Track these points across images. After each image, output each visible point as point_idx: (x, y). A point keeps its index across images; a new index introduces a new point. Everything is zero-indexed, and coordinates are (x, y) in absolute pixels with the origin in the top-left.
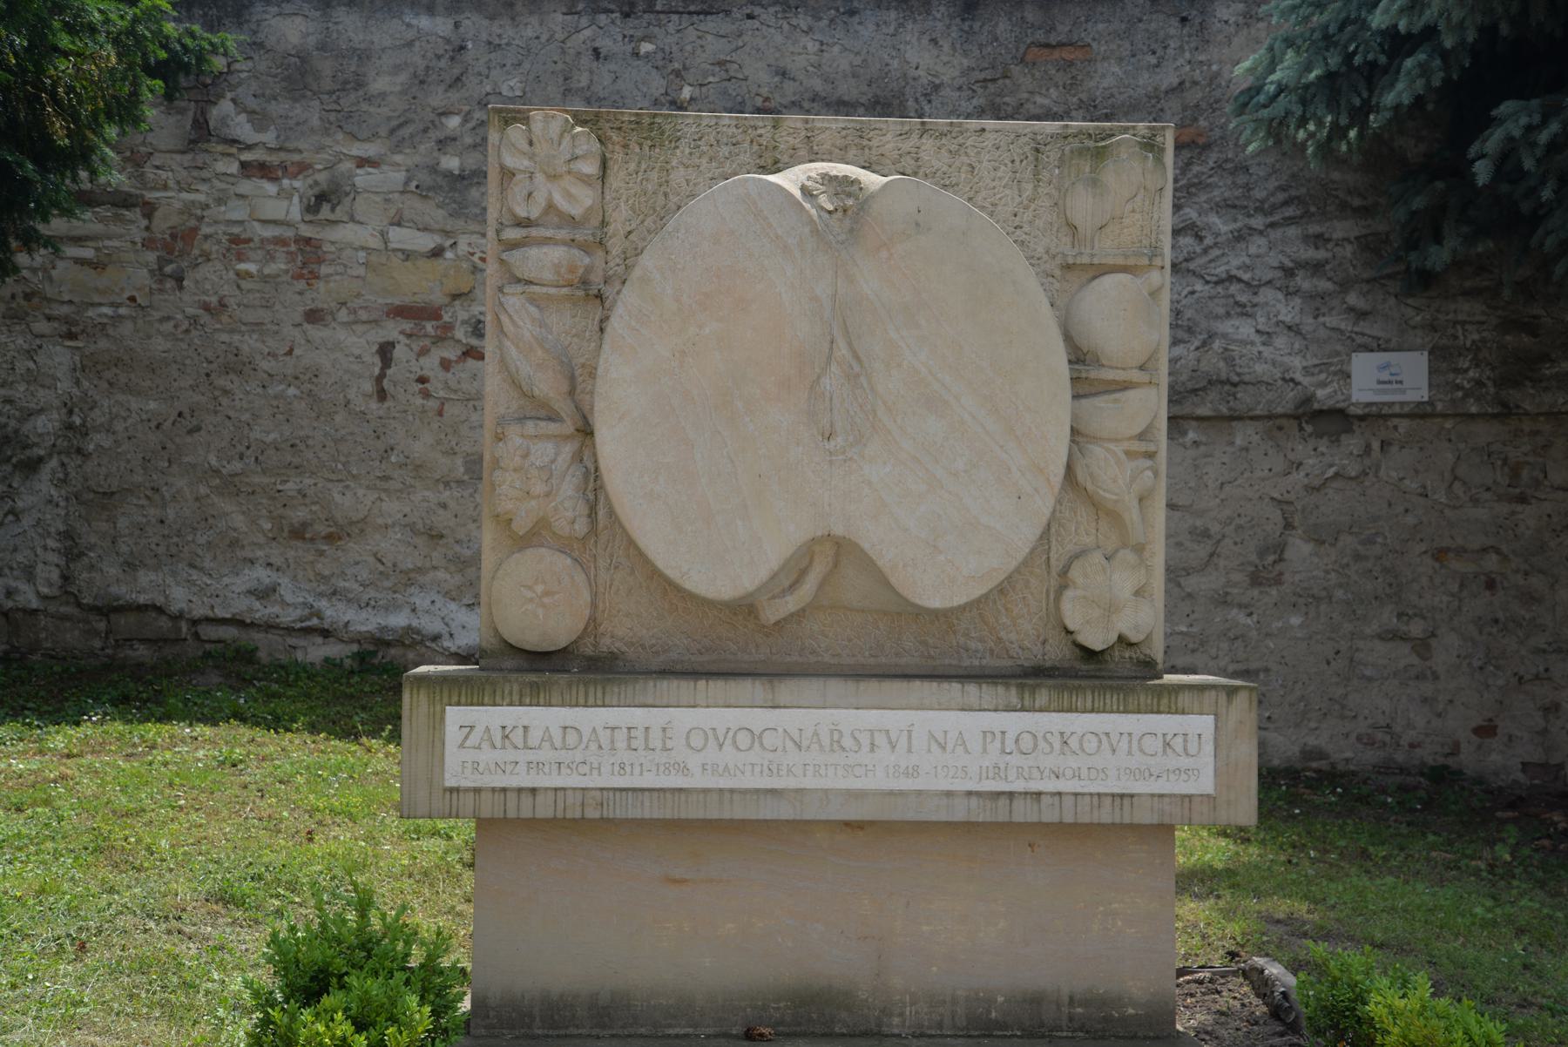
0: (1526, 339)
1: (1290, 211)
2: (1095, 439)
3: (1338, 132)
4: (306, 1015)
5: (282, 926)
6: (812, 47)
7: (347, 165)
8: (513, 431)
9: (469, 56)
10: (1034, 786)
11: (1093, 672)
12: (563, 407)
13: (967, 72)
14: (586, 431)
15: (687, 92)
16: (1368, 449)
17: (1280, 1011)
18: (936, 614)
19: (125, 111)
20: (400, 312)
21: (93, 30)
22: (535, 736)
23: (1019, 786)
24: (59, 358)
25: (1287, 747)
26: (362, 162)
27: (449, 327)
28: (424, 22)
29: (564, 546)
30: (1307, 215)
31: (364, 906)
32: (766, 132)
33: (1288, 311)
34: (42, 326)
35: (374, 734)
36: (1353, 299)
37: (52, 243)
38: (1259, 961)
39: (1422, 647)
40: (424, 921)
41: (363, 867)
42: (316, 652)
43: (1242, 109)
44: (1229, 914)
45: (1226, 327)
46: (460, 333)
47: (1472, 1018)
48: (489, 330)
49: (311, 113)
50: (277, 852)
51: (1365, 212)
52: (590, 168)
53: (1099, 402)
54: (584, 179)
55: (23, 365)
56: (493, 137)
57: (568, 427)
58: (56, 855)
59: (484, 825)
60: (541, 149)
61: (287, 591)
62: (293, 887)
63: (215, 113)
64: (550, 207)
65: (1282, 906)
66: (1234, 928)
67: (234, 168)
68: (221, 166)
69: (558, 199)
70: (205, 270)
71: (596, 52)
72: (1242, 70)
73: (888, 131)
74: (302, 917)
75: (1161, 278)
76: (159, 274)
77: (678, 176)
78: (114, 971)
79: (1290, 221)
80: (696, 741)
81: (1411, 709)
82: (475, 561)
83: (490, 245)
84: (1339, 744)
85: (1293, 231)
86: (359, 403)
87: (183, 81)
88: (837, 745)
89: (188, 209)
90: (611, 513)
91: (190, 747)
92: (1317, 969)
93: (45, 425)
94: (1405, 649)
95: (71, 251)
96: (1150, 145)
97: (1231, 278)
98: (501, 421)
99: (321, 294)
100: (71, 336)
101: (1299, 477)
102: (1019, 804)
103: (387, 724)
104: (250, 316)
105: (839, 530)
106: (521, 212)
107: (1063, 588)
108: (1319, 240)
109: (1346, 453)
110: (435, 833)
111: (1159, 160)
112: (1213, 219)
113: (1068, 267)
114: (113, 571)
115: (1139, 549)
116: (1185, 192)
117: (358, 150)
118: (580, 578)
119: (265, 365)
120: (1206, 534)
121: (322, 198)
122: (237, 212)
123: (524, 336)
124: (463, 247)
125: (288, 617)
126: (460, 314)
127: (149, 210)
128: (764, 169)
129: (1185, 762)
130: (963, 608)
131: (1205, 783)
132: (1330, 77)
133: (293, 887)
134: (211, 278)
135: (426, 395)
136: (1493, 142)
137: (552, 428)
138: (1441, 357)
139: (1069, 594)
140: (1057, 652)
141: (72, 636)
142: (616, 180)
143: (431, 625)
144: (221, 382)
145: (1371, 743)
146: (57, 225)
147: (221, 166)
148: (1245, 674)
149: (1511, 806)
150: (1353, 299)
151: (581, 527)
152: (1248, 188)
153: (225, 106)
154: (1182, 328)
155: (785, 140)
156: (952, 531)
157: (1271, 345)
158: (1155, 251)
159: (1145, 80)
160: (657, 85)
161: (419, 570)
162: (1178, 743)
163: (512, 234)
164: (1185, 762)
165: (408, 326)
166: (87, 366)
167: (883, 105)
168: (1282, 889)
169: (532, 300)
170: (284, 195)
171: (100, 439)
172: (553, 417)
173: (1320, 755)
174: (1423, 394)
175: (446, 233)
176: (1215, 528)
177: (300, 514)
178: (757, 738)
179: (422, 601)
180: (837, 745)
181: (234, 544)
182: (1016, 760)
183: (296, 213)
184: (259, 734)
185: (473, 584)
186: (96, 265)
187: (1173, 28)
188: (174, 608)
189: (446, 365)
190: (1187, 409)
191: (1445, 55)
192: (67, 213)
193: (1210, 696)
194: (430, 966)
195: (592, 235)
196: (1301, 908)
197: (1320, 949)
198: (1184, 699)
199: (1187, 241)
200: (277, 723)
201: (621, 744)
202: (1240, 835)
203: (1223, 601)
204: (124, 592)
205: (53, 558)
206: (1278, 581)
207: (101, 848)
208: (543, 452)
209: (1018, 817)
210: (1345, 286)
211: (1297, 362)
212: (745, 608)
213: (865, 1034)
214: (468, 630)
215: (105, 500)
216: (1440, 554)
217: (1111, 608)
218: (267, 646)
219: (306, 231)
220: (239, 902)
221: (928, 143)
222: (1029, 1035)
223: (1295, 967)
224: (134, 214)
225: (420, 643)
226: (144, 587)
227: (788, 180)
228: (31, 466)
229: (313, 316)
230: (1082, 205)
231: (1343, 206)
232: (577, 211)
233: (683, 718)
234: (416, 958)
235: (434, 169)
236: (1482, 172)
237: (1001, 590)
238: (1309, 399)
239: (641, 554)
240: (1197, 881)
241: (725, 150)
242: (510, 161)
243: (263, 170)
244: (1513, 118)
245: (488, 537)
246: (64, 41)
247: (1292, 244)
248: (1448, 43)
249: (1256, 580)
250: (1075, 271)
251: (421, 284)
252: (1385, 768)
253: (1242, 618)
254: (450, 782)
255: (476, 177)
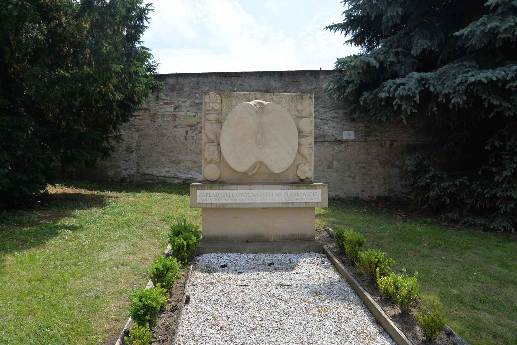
0: (369, 129)
1: (333, 108)
2: (302, 145)
3: (340, 96)
4: (176, 238)
5: (172, 225)
6: (256, 82)
7: (180, 102)
8: (207, 145)
9: (200, 84)
10: (293, 202)
11: (302, 183)
12: (215, 141)
13: (281, 86)
14: (219, 145)
15: (235, 89)
16: (345, 146)
17: (331, 236)
18: (277, 174)
19: (146, 95)
20: (189, 126)
21: (141, 83)
22: (211, 194)
23: (290, 202)
24: (136, 135)
25: (333, 195)
26: (183, 102)
27: (197, 128)
28: (193, 79)
29: (216, 163)
30: (335, 109)
31: (185, 221)
32: (248, 95)
33: (333, 124)
34: (133, 130)
35: (186, 194)
36: (343, 122)
37: (135, 116)
38: (328, 228)
39: (354, 178)
40: (194, 224)
41: (185, 216)
42: (176, 181)
43: (325, 92)
44: (323, 221)
45: (323, 127)
46: (198, 129)
47: (359, 235)
48: (203, 128)
49: (175, 94)
50: (171, 213)
51: (344, 109)
52: (219, 101)
53: (303, 139)
54: (218, 103)
55: (130, 136)
56: (203, 97)
57: (216, 144)
58: (138, 213)
59: (204, 209)
60: (211, 98)
61: (171, 171)
62: (174, 218)
63: (160, 95)
64: (213, 108)
65: (332, 219)
66: (324, 223)
67: (163, 103)
68: (161, 103)
69: (214, 107)
70: (158, 120)
71: (220, 83)
72: (325, 86)
73: (268, 95)
74: (175, 223)
75: (312, 119)
76: (151, 121)
77: (234, 103)
78: (147, 231)
79: (333, 110)
80: (238, 195)
81: (352, 188)
82: (201, 166)
83: (203, 114)
84: (341, 194)
85: (333, 112)
86: (182, 141)
87: (155, 90)
88: (261, 195)
89: (155, 110)
90: (223, 158)
91: (157, 196)
92: (337, 229)
93: (134, 145)
94: (351, 178)
95: (138, 118)
96: (310, 97)
97: (324, 119)
98: (205, 143)
99: (176, 123)
100: (138, 131)
101: (335, 151)
102: (290, 204)
103: (187, 193)
104: (165, 127)
105: (261, 160)
106: (208, 109)
107: (297, 169)
108: (337, 113)
109: (342, 147)
110: (196, 210)
111: (312, 100)
112: (321, 109)
113: (297, 117)
114: (145, 168)
115: (310, 163)
116: (316, 106)
117: (182, 100)
118: (218, 169)
119: (168, 135)
120: (320, 160)
121: (176, 108)
122: (163, 110)
123: (208, 129)
124: (199, 115)
125: (172, 176)
126: (198, 126)
127: (150, 110)
128: (248, 101)
129: (317, 197)
130: (281, 173)
131: (320, 200)
132: (338, 87)
133: (174, 218)
134: (159, 121)
135: (193, 139)
136: (363, 98)
137: (213, 144)
138: (356, 132)
139: (298, 170)
140: (296, 180)
141: (139, 179)
142: (223, 103)
143: (195, 177)
144: (161, 138)
145: (346, 193)
146: (136, 114)
147: (161, 103)
148: (327, 183)
149: (366, 203)
150: (343, 122)
151: (218, 160)
152: (326, 105)
153: (161, 94)
154: (316, 127)
155: (251, 96)
156: (279, 160)
157: (330, 130)
158: (311, 115)
159: (309, 87)
160: (230, 88)
161: (193, 168)
162: (316, 194)
163: (207, 112)
164: (317, 197)
165: (190, 128)
166: (140, 136)
167: (267, 91)
168: (332, 217)
169: (210, 123)
170: (171, 107)
171: (142, 147)
172: (213, 142)
173: (338, 196)
174: (354, 138)
175: (196, 113)
176: (322, 160)
177: (173, 159)
178: (247, 194)
179: (193, 173)
180: (261, 195)
181: (163, 164)
182: (290, 197)
183: (172, 110)
184: (168, 194)
185: (201, 170)
186: (142, 120)
187: (314, 79)
188: (154, 174)
189: (196, 134)
190: (317, 140)
191: (355, 84)
192: (137, 111)
193: (321, 186)
194: (195, 231)
195: (220, 112)
196: (335, 220)
197: (337, 226)
198: (317, 187)
199: (317, 113)
200: (171, 193)
201: (225, 196)
202: (325, 208)
203: (323, 171)
204: (146, 172)
205: (135, 166)
206: (332, 168)
207: (144, 212)
208: (212, 148)
209: (290, 207)
210: (341, 120)
211: (334, 133)
212: (245, 173)
213: (266, 241)
214: (200, 178)
215: (143, 157)
216: (356, 163)
217: (305, 173)
218: (169, 180)
219: (174, 113)
220: (166, 221)
221: (274, 97)
222: (292, 241)
223: (333, 229)
224: (147, 111)
225: (193, 180)
226: (149, 171)
227: (252, 103)
228: (132, 152)
229: (175, 127)
230: (300, 107)
231: (341, 108)
232: (217, 109)
233: (235, 191)
234: (193, 230)
235: (194, 102)
236: (361, 103)
237: (287, 170)
238: (336, 139)
239: (228, 165)
240: (319, 216)
241: (241, 98)
242: (206, 101)
243: (167, 104)
244: (366, 94)
245: (203, 162)
246: (137, 85)
247: (333, 114)
248: (356, 83)
249: (328, 168)
250: (299, 118)
251: (192, 121)
252: (348, 197)
253: (326, 174)
254: (198, 202)
255: (201, 104)
